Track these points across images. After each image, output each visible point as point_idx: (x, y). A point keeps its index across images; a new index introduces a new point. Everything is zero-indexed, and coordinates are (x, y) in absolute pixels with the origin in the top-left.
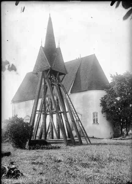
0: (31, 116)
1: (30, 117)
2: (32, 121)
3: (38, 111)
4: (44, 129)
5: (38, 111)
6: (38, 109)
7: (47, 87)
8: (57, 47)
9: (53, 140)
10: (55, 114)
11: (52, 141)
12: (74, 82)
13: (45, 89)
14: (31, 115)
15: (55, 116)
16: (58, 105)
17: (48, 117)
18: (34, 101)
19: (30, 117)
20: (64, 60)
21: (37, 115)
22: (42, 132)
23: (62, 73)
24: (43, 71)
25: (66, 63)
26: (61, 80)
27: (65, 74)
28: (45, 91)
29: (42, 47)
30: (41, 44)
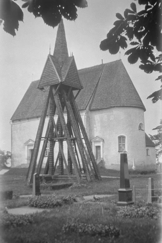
0: (35, 141)
1: (33, 141)
2: (32, 165)
3: (43, 138)
4: (51, 162)
5: (43, 138)
6: (44, 135)
7: (55, 107)
8: (69, 56)
9: (63, 176)
10: (65, 140)
11: (62, 177)
12: (76, 159)
13: (54, 109)
14: (35, 139)
15: (65, 143)
16: (69, 130)
17: (57, 144)
18: (40, 119)
19: (33, 141)
20: (58, 143)
21: (42, 143)
22: (48, 165)
23: (76, 88)
24: (51, 86)
25: (80, 70)
26: (75, 96)
27: (80, 90)
28: (54, 111)
29: (51, 56)
30: (49, 52)
